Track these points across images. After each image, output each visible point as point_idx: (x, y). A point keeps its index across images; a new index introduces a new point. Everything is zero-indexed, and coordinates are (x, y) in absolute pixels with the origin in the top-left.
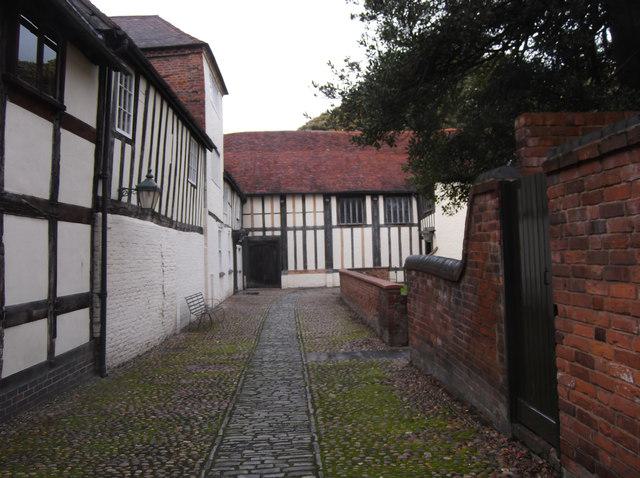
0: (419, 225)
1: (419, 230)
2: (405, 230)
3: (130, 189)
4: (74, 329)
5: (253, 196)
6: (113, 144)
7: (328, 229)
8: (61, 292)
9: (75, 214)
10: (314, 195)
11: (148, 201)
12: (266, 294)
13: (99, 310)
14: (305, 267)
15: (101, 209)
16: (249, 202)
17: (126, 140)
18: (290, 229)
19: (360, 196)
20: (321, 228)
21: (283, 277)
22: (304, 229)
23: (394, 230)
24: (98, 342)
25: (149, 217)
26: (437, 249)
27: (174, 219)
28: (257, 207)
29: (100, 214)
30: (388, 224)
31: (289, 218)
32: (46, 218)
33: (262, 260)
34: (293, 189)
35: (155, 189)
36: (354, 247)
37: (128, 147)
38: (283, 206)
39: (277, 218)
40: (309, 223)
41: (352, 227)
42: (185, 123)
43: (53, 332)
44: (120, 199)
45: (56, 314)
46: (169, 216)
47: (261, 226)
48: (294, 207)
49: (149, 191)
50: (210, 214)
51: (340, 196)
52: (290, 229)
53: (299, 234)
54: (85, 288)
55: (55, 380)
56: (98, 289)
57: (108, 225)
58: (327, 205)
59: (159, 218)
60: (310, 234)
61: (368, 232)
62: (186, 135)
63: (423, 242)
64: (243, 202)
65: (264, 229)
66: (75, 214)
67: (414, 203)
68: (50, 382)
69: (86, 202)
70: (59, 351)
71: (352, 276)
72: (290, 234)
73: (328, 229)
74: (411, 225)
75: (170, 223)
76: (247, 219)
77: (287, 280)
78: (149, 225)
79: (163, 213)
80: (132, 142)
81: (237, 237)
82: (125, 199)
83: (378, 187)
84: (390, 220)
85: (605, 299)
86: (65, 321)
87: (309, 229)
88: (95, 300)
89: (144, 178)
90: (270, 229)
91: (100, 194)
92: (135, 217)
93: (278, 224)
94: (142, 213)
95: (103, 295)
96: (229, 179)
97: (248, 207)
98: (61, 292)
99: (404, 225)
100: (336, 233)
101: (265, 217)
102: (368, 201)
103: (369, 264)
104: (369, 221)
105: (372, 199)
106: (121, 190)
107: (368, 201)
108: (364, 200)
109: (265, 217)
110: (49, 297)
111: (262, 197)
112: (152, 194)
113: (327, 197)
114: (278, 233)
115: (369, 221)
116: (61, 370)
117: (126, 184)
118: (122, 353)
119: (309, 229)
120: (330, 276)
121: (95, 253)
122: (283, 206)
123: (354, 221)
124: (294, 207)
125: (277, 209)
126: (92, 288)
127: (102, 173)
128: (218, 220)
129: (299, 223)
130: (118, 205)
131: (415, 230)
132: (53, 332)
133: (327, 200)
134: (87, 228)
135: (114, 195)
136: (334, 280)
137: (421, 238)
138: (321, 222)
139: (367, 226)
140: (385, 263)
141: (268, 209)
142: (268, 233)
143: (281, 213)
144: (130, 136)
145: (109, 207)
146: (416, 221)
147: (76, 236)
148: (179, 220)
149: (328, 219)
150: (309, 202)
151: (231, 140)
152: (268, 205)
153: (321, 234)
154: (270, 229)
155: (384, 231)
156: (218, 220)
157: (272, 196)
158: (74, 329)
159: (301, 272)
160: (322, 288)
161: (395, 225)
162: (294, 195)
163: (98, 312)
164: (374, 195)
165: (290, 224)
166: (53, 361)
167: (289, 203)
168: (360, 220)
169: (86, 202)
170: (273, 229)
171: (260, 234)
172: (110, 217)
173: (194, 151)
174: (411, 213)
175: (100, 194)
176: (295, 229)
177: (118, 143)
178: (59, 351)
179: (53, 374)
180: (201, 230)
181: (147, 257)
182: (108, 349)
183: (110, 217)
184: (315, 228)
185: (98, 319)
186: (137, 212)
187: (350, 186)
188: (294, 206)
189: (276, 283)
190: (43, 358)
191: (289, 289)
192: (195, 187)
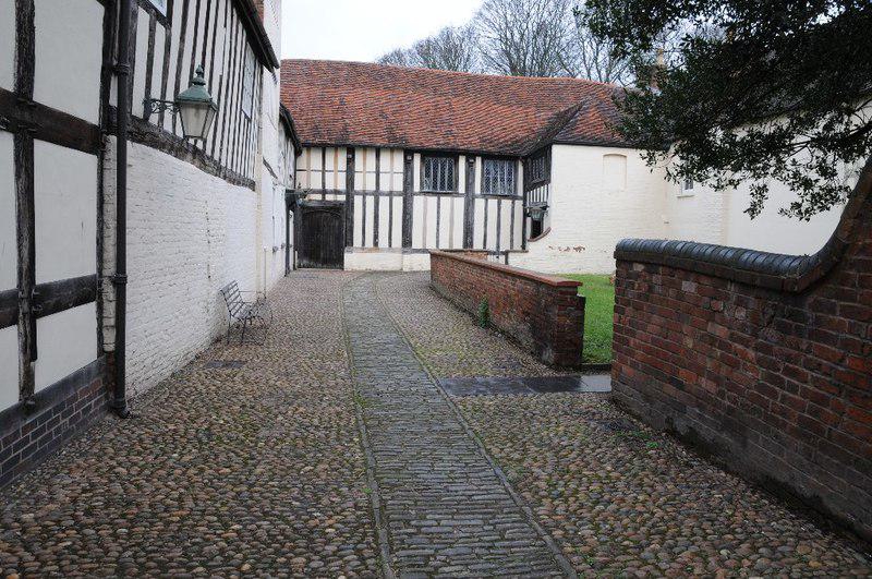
0: (524, 199)
1: (524, 205)
2: (506, 203)
3: (163, 101)
4: (68, 343)
5: (309, 147)
6: (135, 15)
7: (407, 194)
8: (43, 277)
9: (68, 132)
10: (392, 150)
11: (194, 122)
12: (324, 276)
13: (113, 304)
14: (376, 244)
15: (111, 132)
16: (304, 153)
17: (158, 16)
18: (358, 193)
19: (453, 154)
20: (399, 194)
21: (346, 255)
22: (377, 194)
23: (493, 203)
24: (112, 362)
25: (189, 156)
26: (549, 230)
27: (223, 164)
28: (315, 159)
29: (113, 139)
30: (486, 196)
31: (358, 179)
32: (12, 132)
33: (320, 233)
34: (366, 140)
35: (209, 106)
36: (440, 221)
37: (160, 29)
38: (350, 161)
39: (342, 177)
40: (384, 187)
41: (438, 195)
42: (241, 17)
43: (30, 350)
44: (146, 118)
45: (33, 318)
46: (216, 157)
47: (320, 187)
48: (364, 164)
49: (198, 107)
50: (265, 163)
51: (426, 154)
52: (358, 193)
53: (370, 200)
54: (88, 268)
55: (35, 435)
56: (110, 268)
57: (129, 161)
58: (408, 164)
59: (199, 157)
60: (384, 201)
61: (460, 203)
62: (242, 37)
63: (529, 220)
64: (298, 153)
65: (324, 192)
66: (68, 132)
67: (521, 169)
68: (26, 440)
69: (90, 113)
70: (42, 383)
71: (461, 261)
72: (358, 200)
73: (407, 194)
74: (514, 198)
75: (218, 170)
76: (301, 177)
77: (352, 259)
78: (187, 168)
79: (208, 152)
80: (167, 21)
81: (292, 200)
82: (154, 119)
83: (474, 144)
84: (488, 190)
85: (657, 287)
86: (50, 328)
87: (384, 194)
88: (104, 289)
89: (184, 87)
90: (331, 192)
91: (113, 101)
92: (169, 153)
93: (342, 186)
94: (179, 148)
95: (120, 283)
96: (286, 121)
97: (303, 161)
98: (43, 277)
99: (505, 197)
100: (418, 201)
101: (324, 175)
102: (462, 161)
103: (458, 244)
104: (462, 189)
105: (467, 160)
106: (148, 102)
107: (462, 161)
108: (457, 161)
109: (324, 175)
110: (19, 286)
111: (323, 148)
112: (203, 113)
113: (409, 153)
114: (342, 198)
115: (462, 189)
116: (48, 415)
117: (156, 93)
118: (150, 374)
119: (384, 194)
120: (407, 257)
121: (105, 206)
122: (350, 161)
123: (442, 187)
124: (364, 164)
125: (342, 164)
126: (100, 269)
127: (116, 64)
128: (272, 173)
129: (371, 187)
130: (144, 129)
131: (519, 204)
132: (30, 350)
133: (409, 158)
134: (91, 160)
135: (137, 109)
136: (423, 263)
137: (526, 215)
138: (399, 187)
139: (458, 195)
140: (478, 245)
141: (330, 165)
142: (329, 197)
143: (347, 171)
144: (164, 11)
145: (129, 128)
146: (520, 193)
147: (65, 173)
148: (229, 167)
149: (408, 182)
150: (385, 157)
151: (283, 62)
152: (330, 156)
153: (398, 202)
154: (331, 192)
155: (479, 203)
156: (272, 173)
157: (336, 147)
158: (68, 343)
159: (370, 250)
160: (395, 272)
161: (495, 196)
162: (365, 148)
163: (110, 309)
164: (471, 156)
165: (358, 186)
166: (30, 401)
167: (359, 157)
168: (450, 187)
169: (90, 113)
170: (337, 192)
171: (319, 197)
172: (132, 148)
173: (250, 62)
174: (516, 182)
175: (113, 101)
176: (364, 194)
177: (143, 18)
178: (42, 383)
179: (33, 425)
180: (252, 185)
181: (187, 220)
182: (129, 370)
183: (132, 148)
184: (391, 194)
185: (112, 322)
186: (172, 146)
187: (436, 141)
188: (365, 163)
189: (336, 261)
190: (43, 324)
191: (353, 271)
192: (250, 120)
